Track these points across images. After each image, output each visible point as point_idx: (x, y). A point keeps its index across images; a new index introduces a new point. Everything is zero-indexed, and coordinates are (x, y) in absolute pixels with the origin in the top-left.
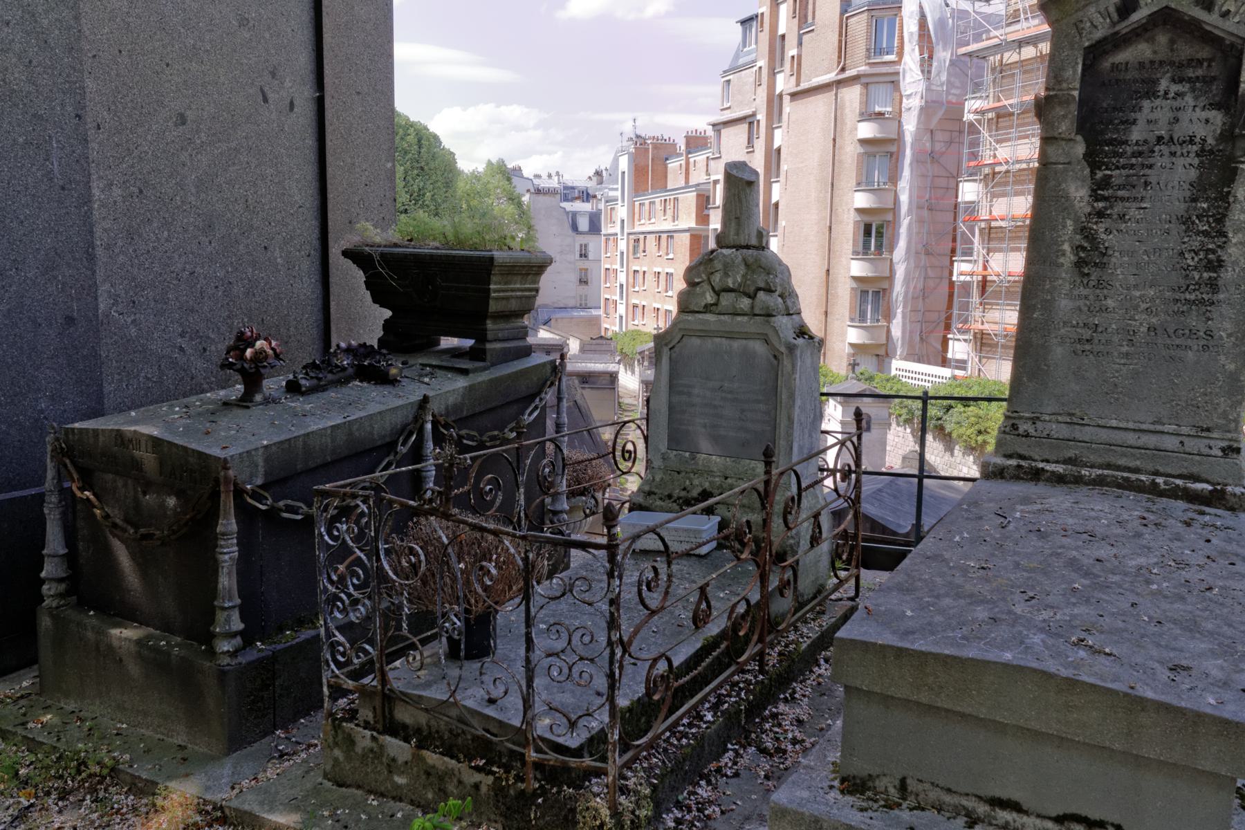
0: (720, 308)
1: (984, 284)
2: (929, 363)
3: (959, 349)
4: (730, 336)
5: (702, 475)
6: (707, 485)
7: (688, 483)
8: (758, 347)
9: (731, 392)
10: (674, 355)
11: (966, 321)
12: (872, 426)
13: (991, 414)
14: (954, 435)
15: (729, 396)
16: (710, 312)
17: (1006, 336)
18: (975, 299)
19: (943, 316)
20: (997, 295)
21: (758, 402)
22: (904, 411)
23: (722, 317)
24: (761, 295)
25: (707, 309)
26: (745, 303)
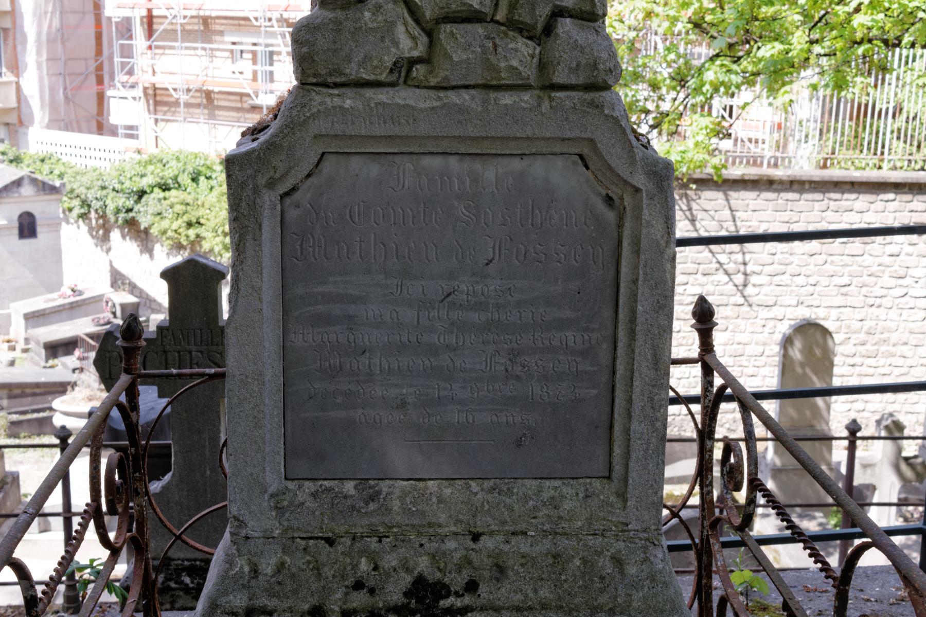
0: (443, 73)
1: (150, 21)
2: (80, 131)
3: (124, 107)
4: (476, 151)
5: (402, 540)
6: (423, 564)
7: (364, 565)
8: (561, 176)
9: (479, 306)
10: (293, 214)
11: (130, 73)
12: (39, 229)
13: (202, 198)
14: (154, 231)
15: (475, 317)
16: (407, 81)
17: (189, 90)
18: (139, 40)
19: (93, 65)
20: (170, 34)
21: (562, 324)
22: (76, 203)
23: (453, 97)
24: (566, 26)
25: (403, 72)
26: (520, 54)
